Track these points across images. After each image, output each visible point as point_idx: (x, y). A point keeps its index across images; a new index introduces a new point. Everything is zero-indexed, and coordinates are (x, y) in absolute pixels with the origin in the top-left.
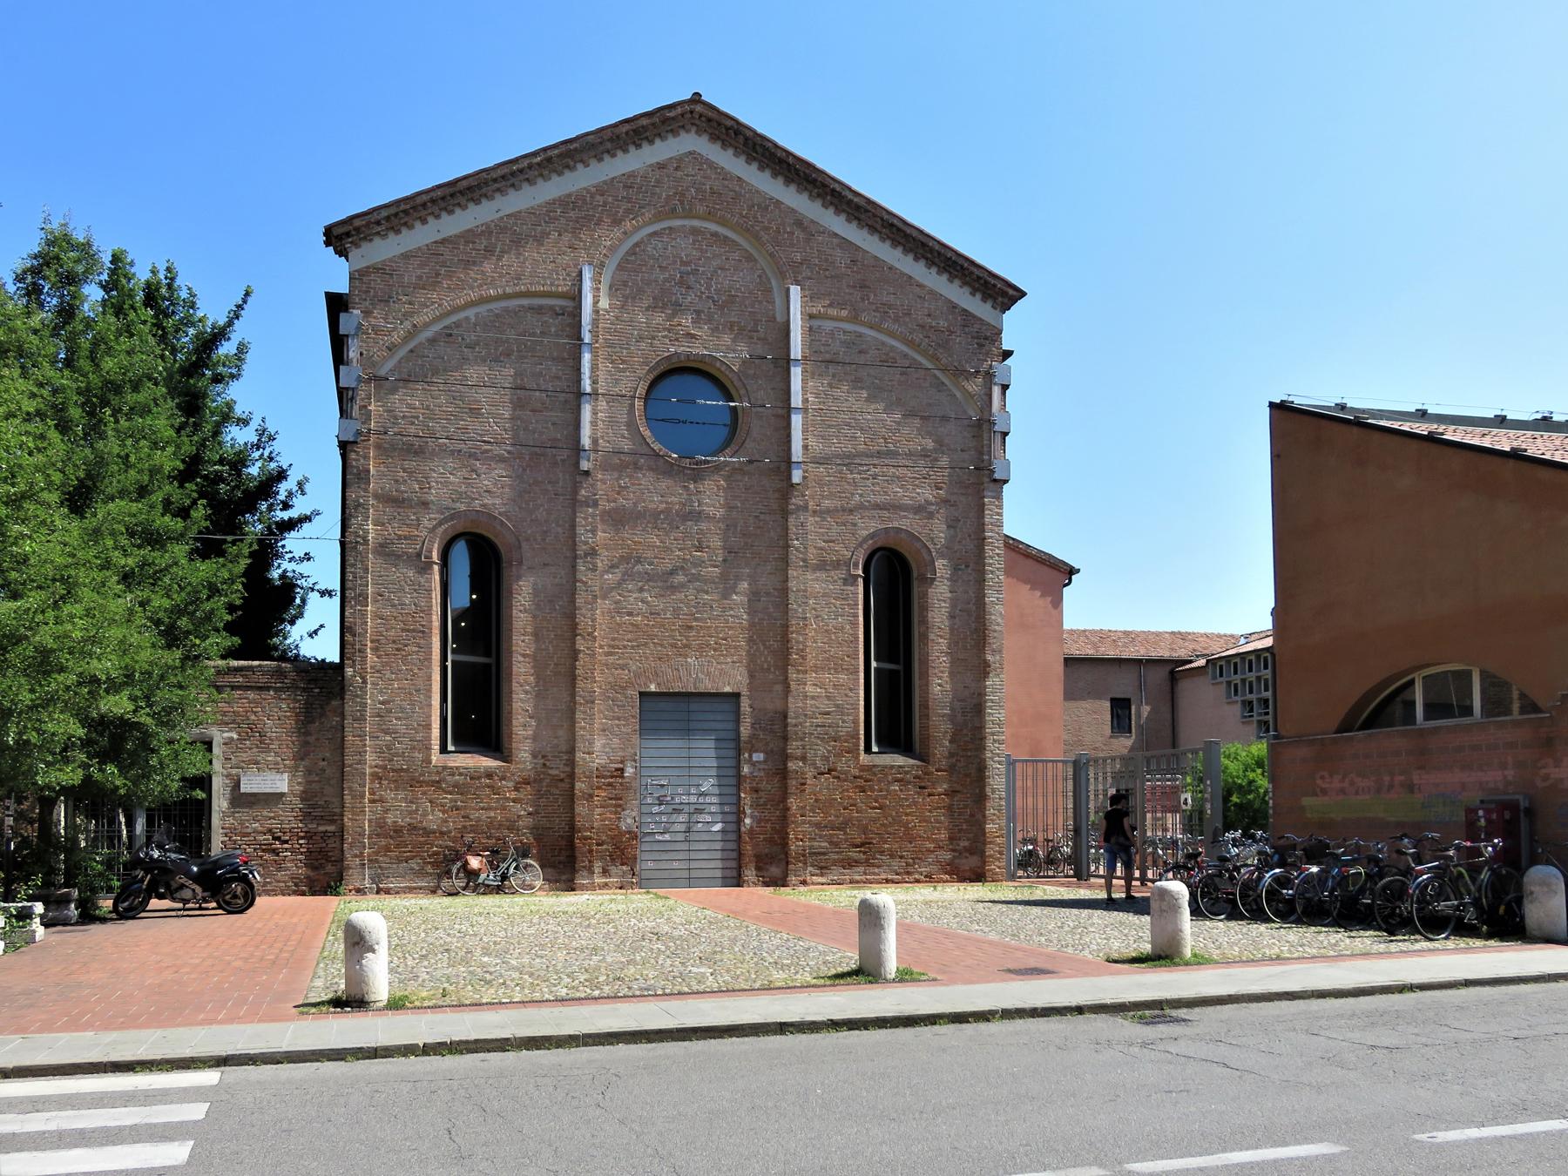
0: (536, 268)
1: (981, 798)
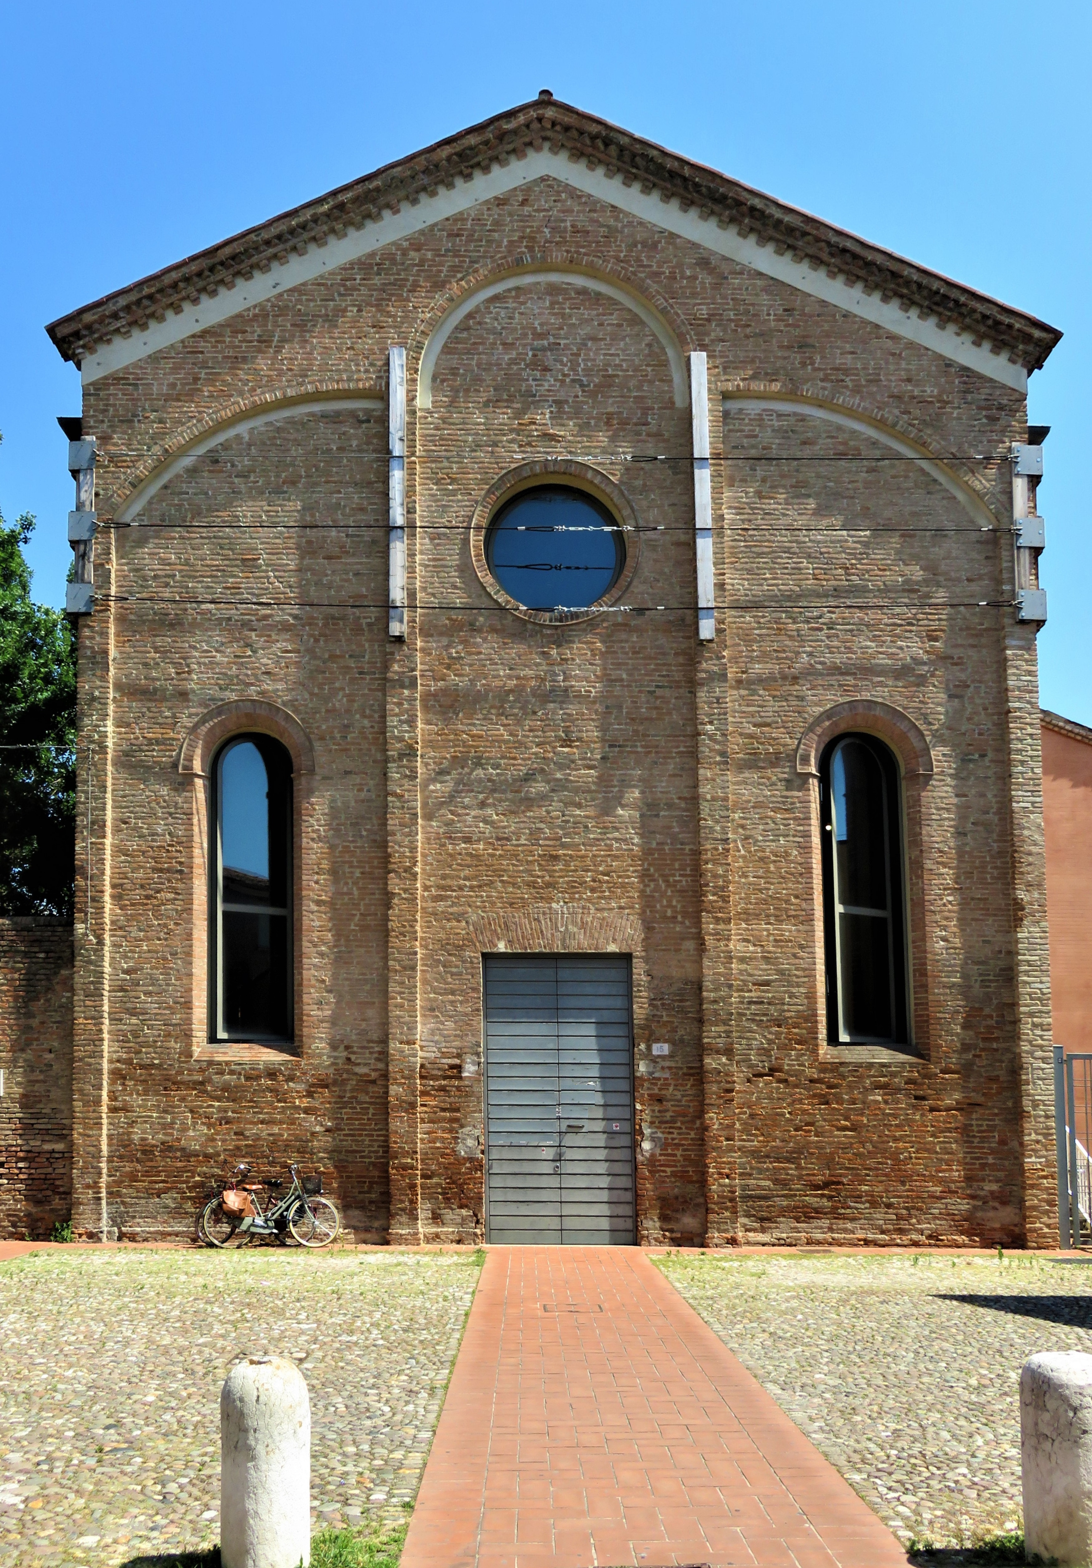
0: (326, 360)
1: (1016, 1116)
